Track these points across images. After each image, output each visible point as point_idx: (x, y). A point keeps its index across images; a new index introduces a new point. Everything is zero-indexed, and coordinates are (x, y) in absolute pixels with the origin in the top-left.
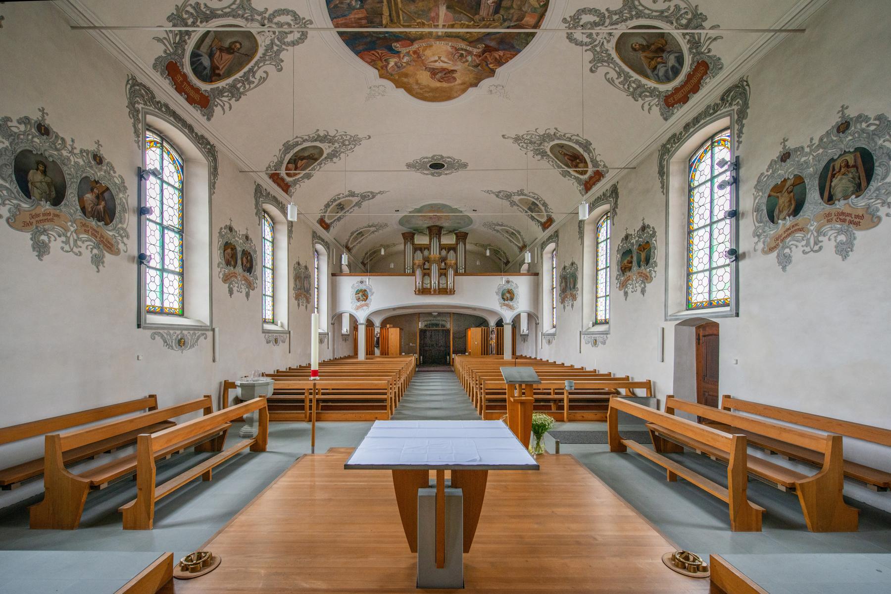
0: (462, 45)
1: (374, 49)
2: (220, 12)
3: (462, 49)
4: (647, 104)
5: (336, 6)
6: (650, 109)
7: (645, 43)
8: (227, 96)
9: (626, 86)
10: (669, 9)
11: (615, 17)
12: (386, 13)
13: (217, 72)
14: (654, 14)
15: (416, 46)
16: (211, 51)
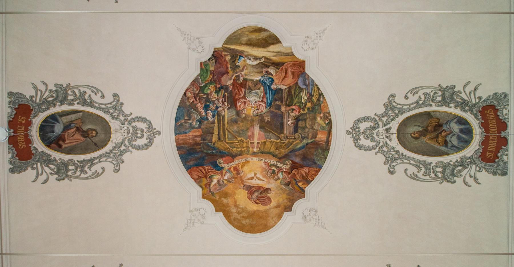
0: (273, 161)
1: (202, 165)
2: (97, 105)
3: (274, 165)
4: (467, 177)
6: (476, 180)
7: (421, 129)
8: (52, 169)
9: (432, 175)
10: (420, 98)
11: (385, 119)
12: (216, 132)
13: (61, 142)
14: (412, 106)
15: (236, 162)
16: (70, 125)
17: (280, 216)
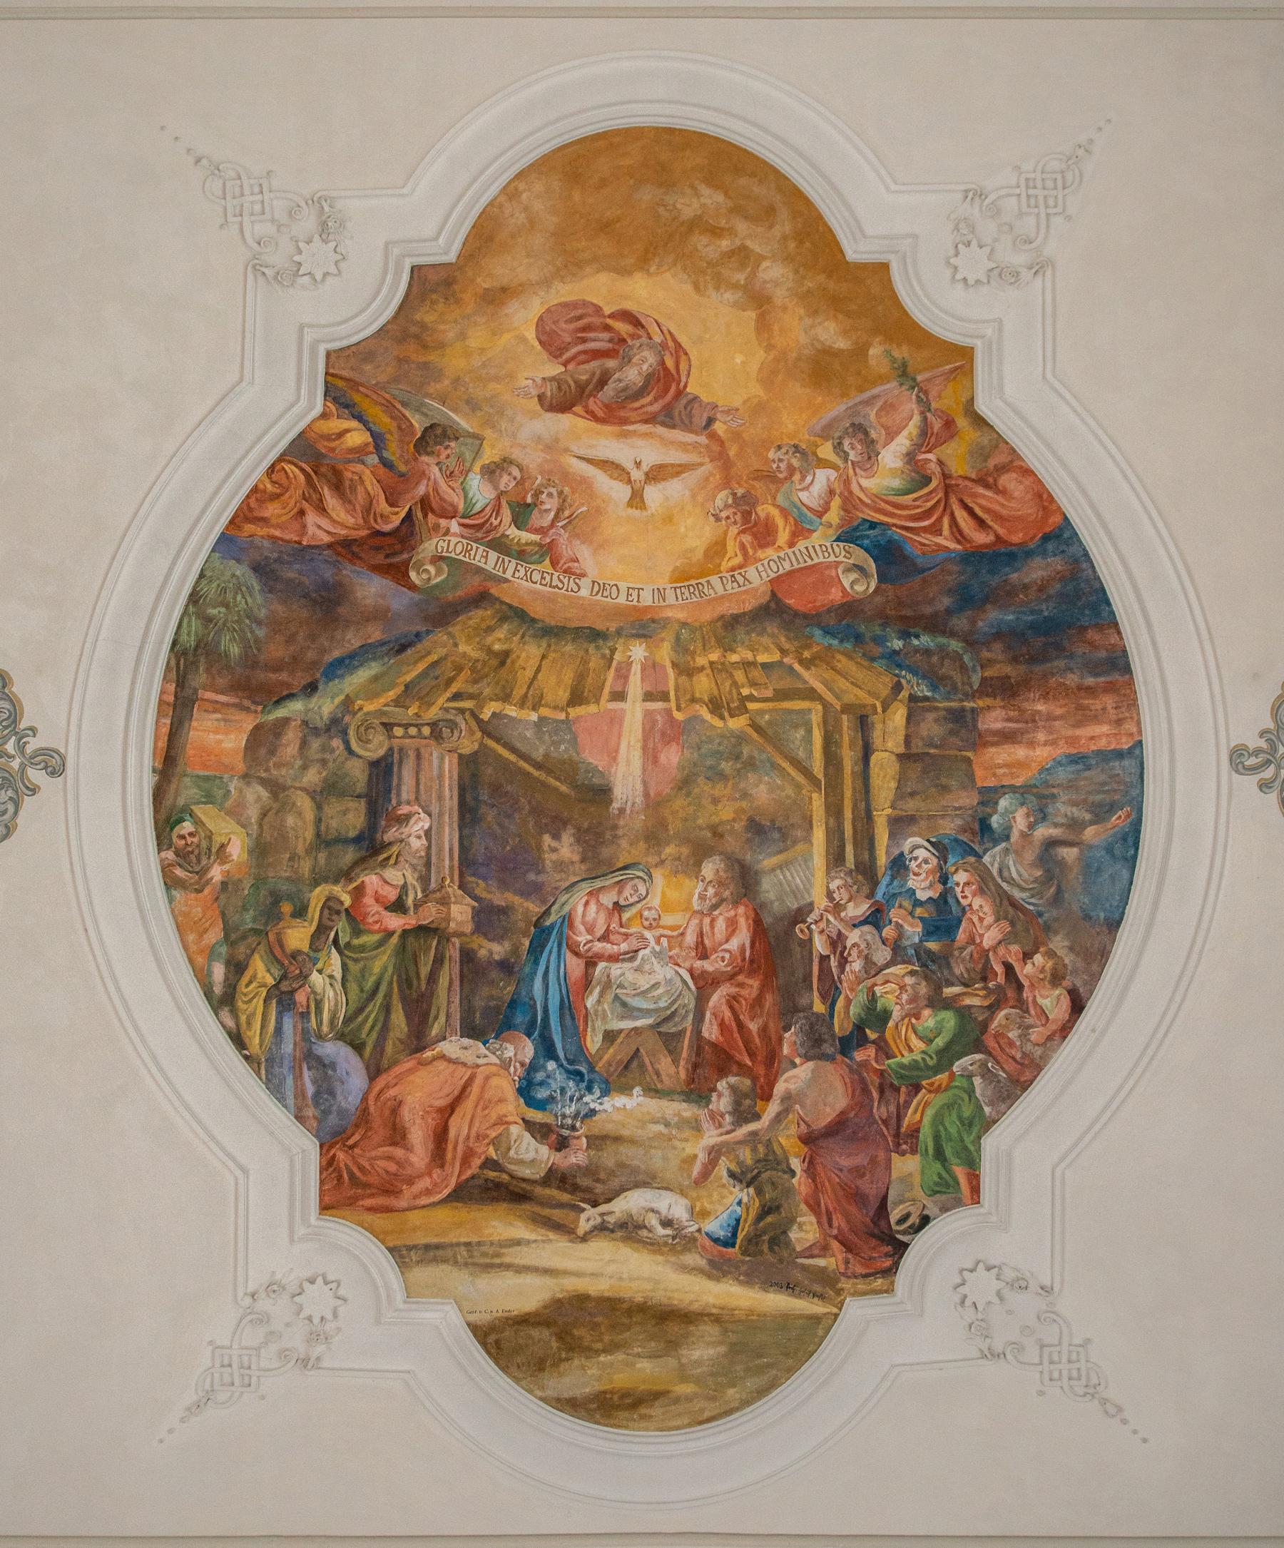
1: (974, 558)
3: (521, 555)
5: (1101, 812)
12: (884, 768)
15: (758, 577)
17: (485, 235)
